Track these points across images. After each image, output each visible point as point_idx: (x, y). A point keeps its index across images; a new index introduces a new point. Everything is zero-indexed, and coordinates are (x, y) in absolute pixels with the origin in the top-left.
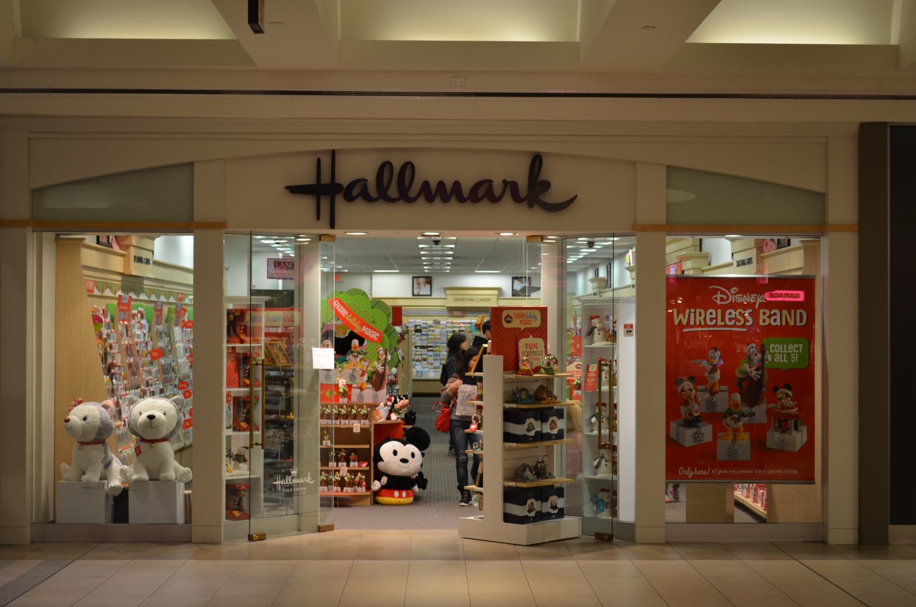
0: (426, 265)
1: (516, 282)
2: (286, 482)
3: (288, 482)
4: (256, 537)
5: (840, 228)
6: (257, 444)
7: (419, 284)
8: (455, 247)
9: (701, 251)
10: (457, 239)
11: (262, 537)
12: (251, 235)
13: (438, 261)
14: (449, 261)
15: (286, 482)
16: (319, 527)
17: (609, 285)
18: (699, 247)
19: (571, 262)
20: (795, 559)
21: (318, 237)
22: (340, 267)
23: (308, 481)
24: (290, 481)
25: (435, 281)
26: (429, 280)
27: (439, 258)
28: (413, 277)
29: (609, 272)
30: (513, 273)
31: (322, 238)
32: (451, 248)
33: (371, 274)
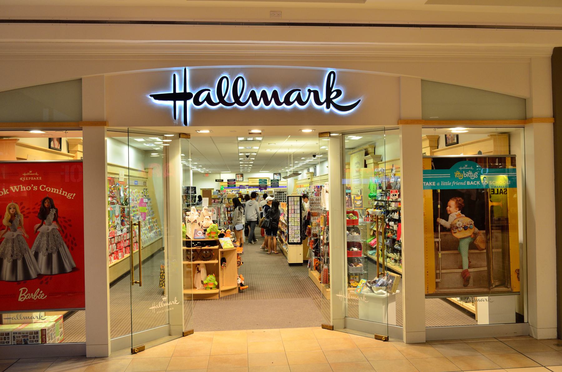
0: (241, 169)
1: (275, 175)
2: (159, 306)
3: (161, 306)
4: (137, 350)
5: (542, 120)
6: (136, 282)
7: (238, 177)
8: (255, 159)
9: (375, 154)
10: (256, 155)
11: (142, 349)
12: (128, 132)
13: (246, 167)
14: (250, 167)
15: (159, 306)
16: (183, 333)
17: (315, 175)
18: (374, 153)
19: (299, 166)
20: (543, 366)
21: (179, 134)
22: (208, 170)
23: (175, 303)
24: (162, 305)
25: (244, 176)
26: (242, 175)
27: (247, 165)
28: (236, 174)
29: (315, 169)
30: (274, 172)
31: (181, 136)
32: (253, 160)
33: (220, 173)
